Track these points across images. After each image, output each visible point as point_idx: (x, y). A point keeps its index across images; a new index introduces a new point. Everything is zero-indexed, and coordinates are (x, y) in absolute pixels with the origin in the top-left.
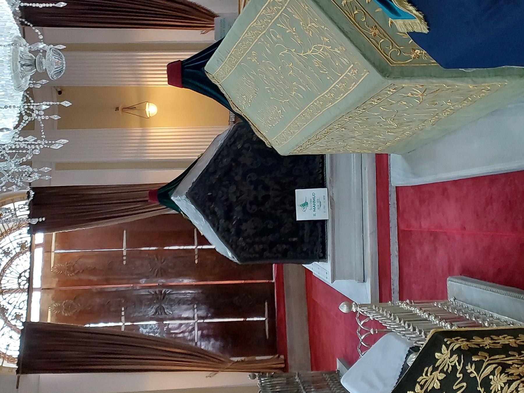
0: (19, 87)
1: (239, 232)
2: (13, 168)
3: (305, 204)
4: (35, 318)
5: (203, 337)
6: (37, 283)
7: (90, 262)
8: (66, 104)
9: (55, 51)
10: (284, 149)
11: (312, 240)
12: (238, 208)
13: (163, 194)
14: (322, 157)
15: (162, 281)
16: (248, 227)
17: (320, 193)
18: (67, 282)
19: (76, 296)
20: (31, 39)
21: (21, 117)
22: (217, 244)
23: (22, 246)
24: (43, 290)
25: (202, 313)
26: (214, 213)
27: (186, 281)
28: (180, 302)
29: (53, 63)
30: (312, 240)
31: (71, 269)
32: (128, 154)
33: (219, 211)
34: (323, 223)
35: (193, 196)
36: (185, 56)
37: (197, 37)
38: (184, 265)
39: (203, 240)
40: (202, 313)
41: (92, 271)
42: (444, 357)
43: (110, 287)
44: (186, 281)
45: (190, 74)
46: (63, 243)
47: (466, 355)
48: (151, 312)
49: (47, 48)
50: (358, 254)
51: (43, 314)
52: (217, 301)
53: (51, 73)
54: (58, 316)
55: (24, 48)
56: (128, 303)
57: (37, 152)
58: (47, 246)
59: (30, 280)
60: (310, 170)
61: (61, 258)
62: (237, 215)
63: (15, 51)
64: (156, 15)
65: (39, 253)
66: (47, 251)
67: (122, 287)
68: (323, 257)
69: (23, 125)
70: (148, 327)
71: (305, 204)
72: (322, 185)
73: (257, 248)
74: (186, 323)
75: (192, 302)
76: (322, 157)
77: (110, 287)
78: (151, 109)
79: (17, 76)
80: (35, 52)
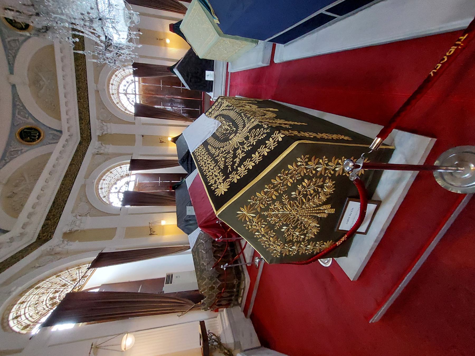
0: (127, 25)
1: (190, 81)
2: (128, 53)
3: (208, 75)
4: (138, 102)
5: (183, 113)
6: (137, 93)
7: (152, 88)
8: (141, 33)
9: (136, 14)
10: (201, 57)
11: (209, 86)
12: (190, 74)
13: (171, 69)
14: (214, 61)
15: (172, 96)
16: (193, 80)
17: (212, 72)
18: (146, 92)
19: (149, 98)
20: (129, 9)
21: (128, 36)
22: (187, 87)
23: (132, 80)
24: (139, 95)
25: (183, 106)
26: (184, 74)
27: (179, 97)
28: (178, 103)
29: (136, 18)
30: (209, 86)
31: (146, 89)
32: (161, 55)
33: (185, 75)
34: (212, 81)
35: (178, 69)
36: (174, 22)
37: (178, 16)
38: (178, 92)
39: (183, 86)
40: (183, 106)
41: (152, 91)
42: (219, 100)
43: (157, 96)
44: (179, 97)
45: (175, 28)
46: (144, 81)
47: (222, 99)
48: (169, 105)
49: (134, 13)
50: (220, 91)
51: (140, 101)
52: (187, 103)
53: (136, 22)
54: (144, 102)
55: (127, 11)
56: (164, 102)
57: (133, 48)
58: (139, 82)
59: (135, 91)
60: (209, 65)
61: (143, 86)
62: (190, 76)
63: (124, 12)
64: (170, 6)
65: (137, 83)
66: (139, 83)
67: (162, 97)
68: (212, 91)
69: (129, 38)
70: (169, 108)
71: (208, 75)
72: (213, 71)
73: (195, 86)
74: (179, 108)
75: (180, 103)
76: (214, 61)
77: (157, 96)
78: (168, 41)
79: (126, 21)
80: (130, 14)
